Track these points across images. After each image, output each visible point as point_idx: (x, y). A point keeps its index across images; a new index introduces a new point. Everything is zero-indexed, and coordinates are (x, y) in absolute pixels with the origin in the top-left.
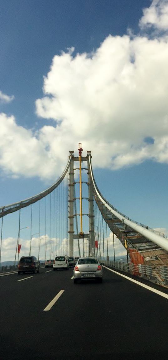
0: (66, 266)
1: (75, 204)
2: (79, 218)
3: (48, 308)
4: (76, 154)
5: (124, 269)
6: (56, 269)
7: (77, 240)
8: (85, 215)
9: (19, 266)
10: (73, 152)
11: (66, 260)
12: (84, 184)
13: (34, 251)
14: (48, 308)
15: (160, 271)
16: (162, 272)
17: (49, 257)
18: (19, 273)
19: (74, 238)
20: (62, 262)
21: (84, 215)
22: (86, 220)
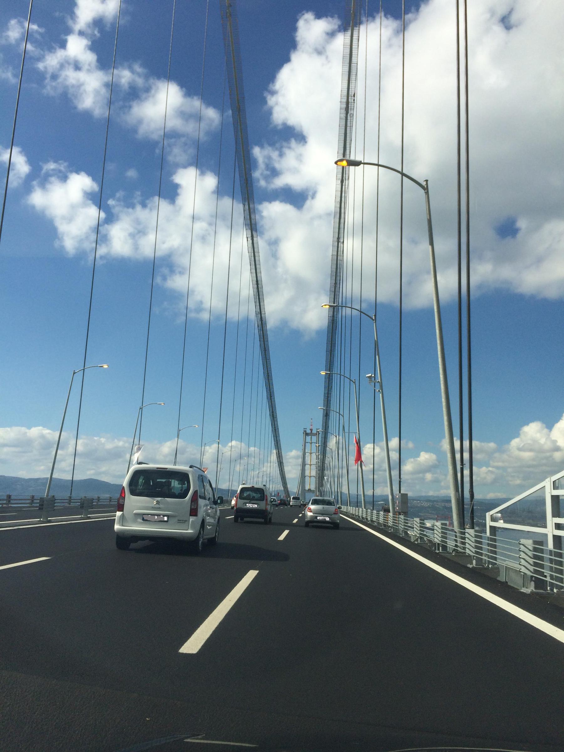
3: (193, 645)
6: (126, 541)
14: (193, 645)
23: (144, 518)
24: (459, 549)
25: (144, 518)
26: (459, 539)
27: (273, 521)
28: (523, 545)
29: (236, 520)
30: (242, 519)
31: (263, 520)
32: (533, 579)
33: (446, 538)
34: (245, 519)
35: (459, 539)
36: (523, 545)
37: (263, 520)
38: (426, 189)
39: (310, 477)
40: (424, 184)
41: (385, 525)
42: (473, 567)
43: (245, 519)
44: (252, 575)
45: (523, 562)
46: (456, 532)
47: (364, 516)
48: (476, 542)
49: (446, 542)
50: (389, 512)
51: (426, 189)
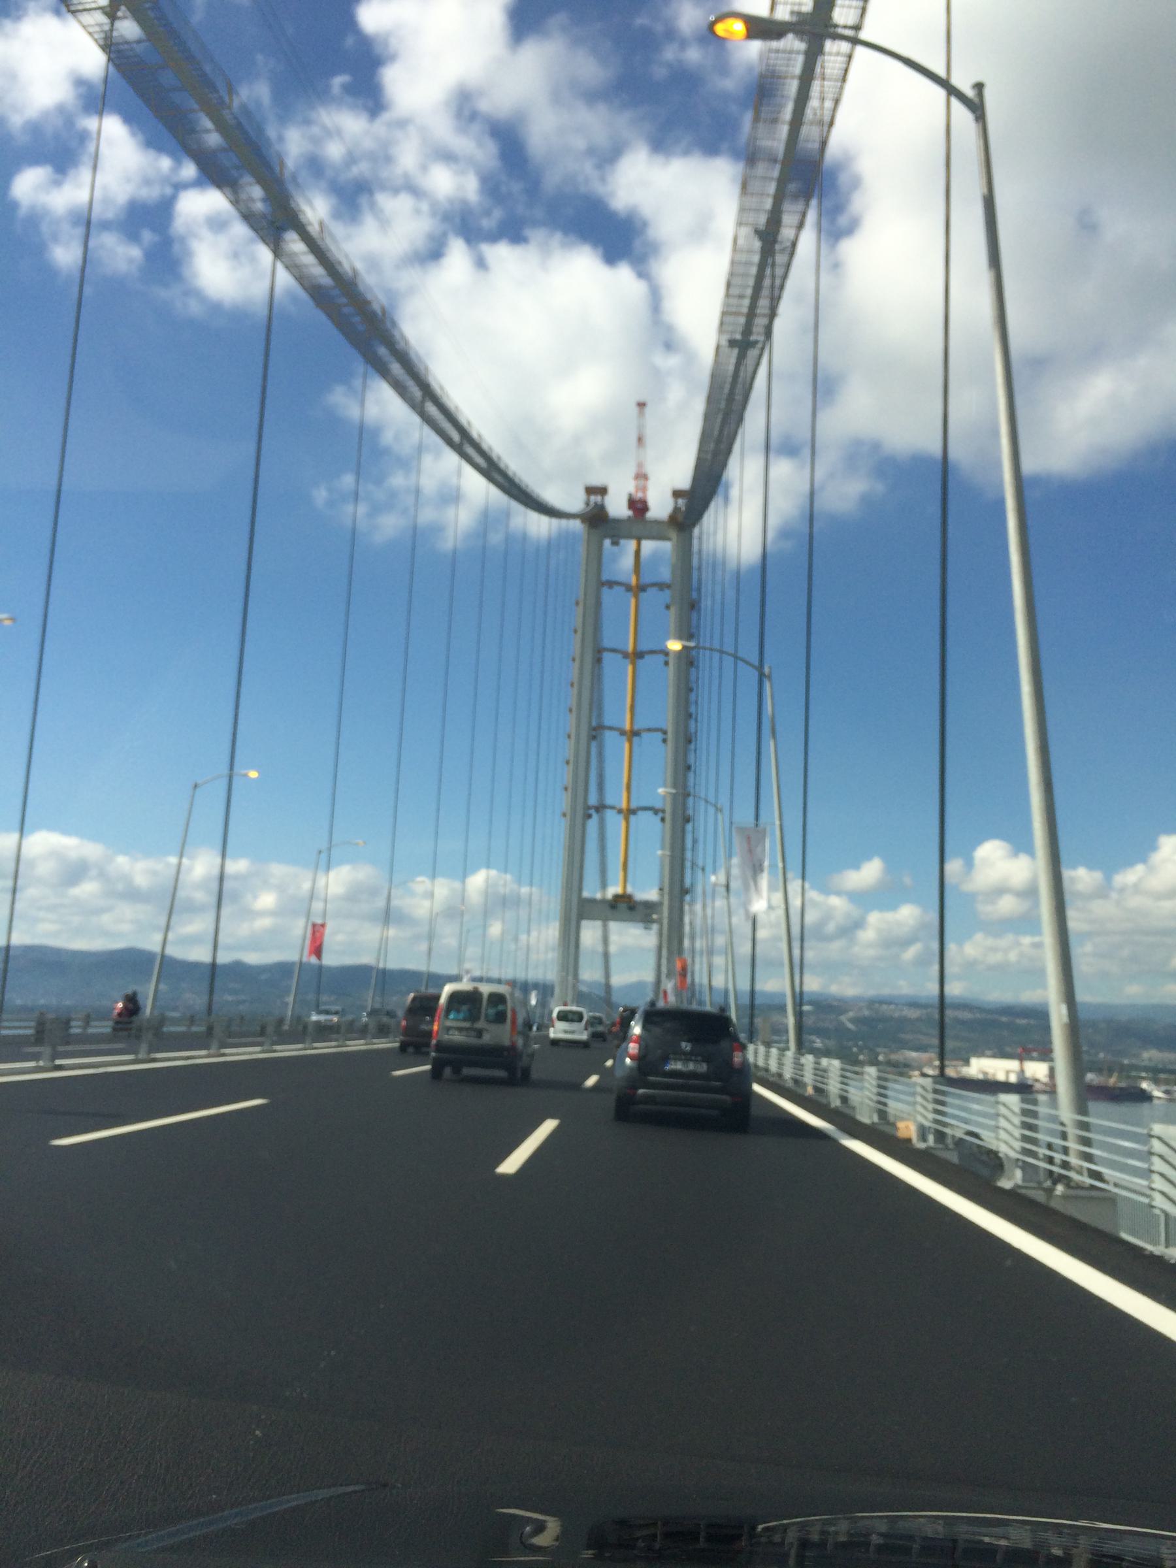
0: (584, 1036)
1: (600, 755)
2: (615, 823)
3: (510, 1165)
4: (617, 507)
5: (796, 1081)
6: (555, 1043)
7: (598, 923)
8: (650, 734)
9: (404, 1023)
10: (603, 491)
11: (584, 1022)
12: (651, 741)
13: (340, 937)
14: (510, 1165)
15: (998, 1115)
16: (925, 1103)
17: (158, 937)
18: (403, 1047)
19: (581, 916)
20: (575, 1026)
21: (644, 735)
22: (650, 835)
23: (566, 1032)
24: (1073, 1175)
25: (566, 1032)
26: (1073, 1145)
27: (535, 1075)
28: (1159, 1138)
29: (436, 1073)
30: (457, 1070)
31: (501, 1074)
32: (1020, 1164)
33: (885, 1096)
34: (467, 1071)
35: (1073, 1145)
36: (1159, 1138)
37: (501, 1074)
38: (977, 107)
39: (638, 655)
40: (970, 93)
41: (796, 1081)
42: (928, 1148)
43: (467, 1071)
44: (548, 1126)
45: (1003, 1135)
46: (1062, 1124)
47: (761, 1063)
48: (879, 1086)
49: (885, 1104)
50: (788, 1049)
51: (977, 107)
